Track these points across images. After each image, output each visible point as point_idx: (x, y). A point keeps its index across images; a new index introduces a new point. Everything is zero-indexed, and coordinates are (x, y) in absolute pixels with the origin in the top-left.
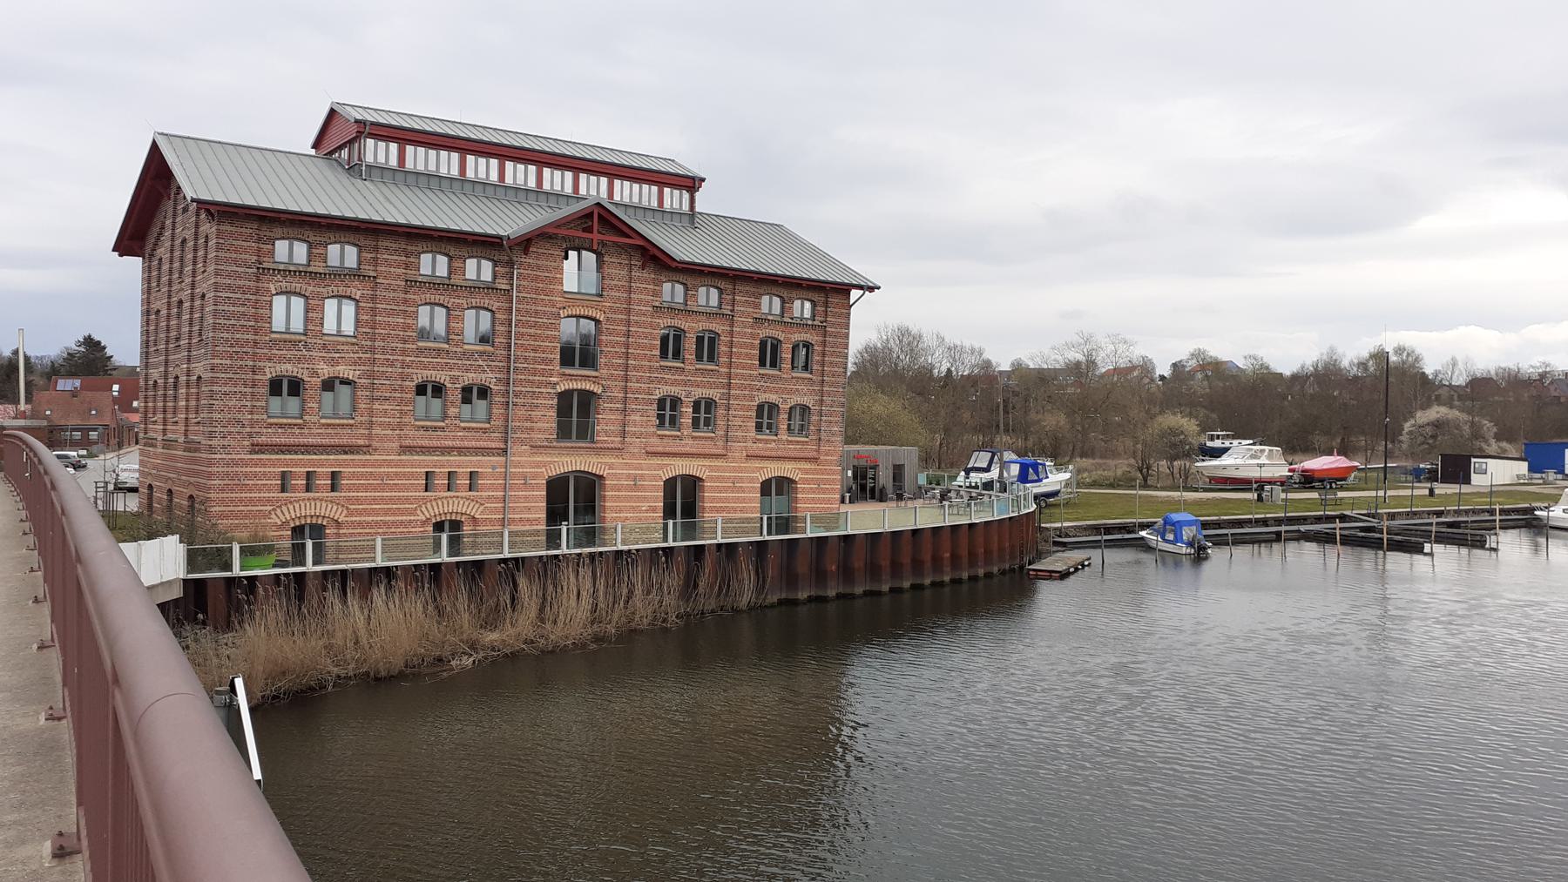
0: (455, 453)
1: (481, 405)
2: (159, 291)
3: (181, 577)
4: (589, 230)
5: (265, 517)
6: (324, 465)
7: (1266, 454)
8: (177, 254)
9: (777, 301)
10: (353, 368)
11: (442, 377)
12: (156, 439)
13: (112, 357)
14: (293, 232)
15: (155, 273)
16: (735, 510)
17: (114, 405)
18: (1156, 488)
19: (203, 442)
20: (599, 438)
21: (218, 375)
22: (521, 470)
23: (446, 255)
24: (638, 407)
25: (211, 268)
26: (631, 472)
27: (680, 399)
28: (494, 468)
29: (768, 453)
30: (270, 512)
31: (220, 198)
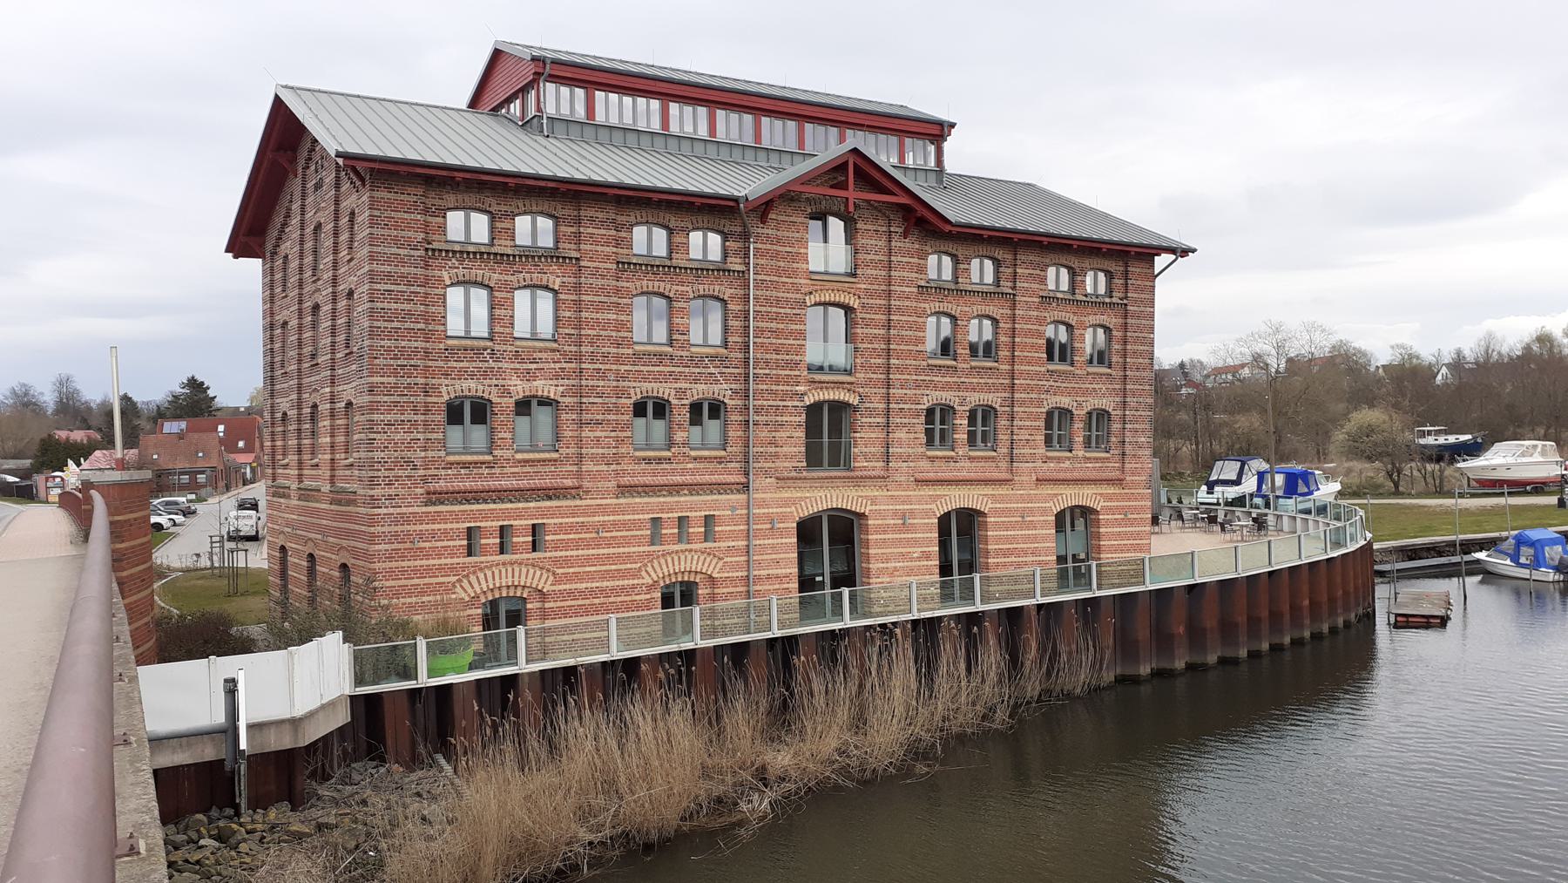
0: (686, 492)
1: (713, 427)
2: (286, 296)
3: (347, 692)
4: (843, 186)
5: (447, 591)
6: (521, 515)
7: (1539, 449)
8: (309, 245)
9: (1064, 274)
10: (555, 382)
11: (665, 390)
12: (289, 488)
13: (215, 397)
14: (470, 199)
15: (278, 276)
16: (1025, 552)
17: (221, 445)
18: (1410, 496)
19: (360, 492)
20: (857, 464)
21: (378, 398)
22: (766, 511)
23: (666, 227)
24: (904, 420)
25: (363, 252)
26: (898, 507)
27: (953, 407)
28: (733, 508)
29: (1062, 476)
30: (454, 586)
31: (372, 151)
